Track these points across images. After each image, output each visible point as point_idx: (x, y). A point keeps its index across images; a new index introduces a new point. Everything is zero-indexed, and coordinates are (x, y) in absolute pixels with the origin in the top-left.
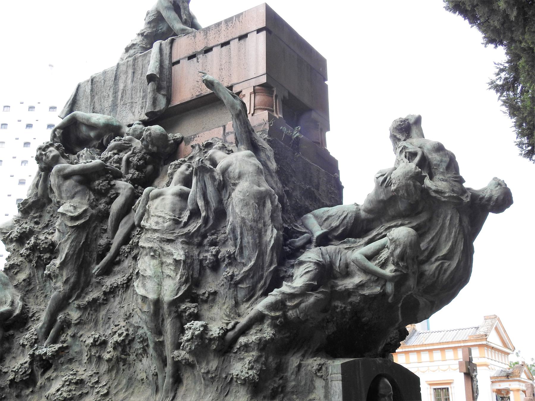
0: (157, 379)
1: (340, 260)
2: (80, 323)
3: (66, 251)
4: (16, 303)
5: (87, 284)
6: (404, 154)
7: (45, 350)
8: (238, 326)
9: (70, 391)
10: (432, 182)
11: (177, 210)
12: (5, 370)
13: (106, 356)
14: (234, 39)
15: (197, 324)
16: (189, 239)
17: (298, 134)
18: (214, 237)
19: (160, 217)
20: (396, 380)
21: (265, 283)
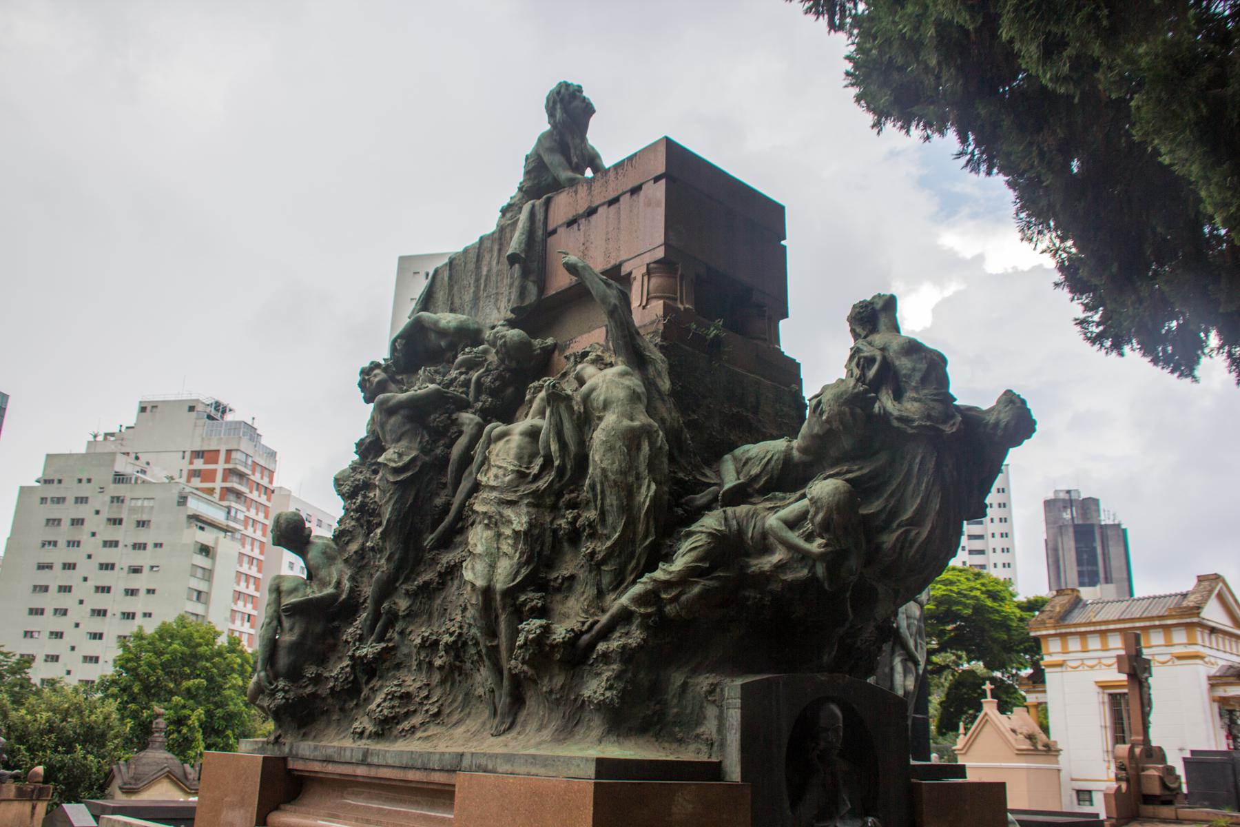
5: (419, 561)
7: (365, 651)
9: (393, 707)
12: (327, 674)
13: (438, 662)
14: (624, 193)
15: (533, 626)
16: (537, 500)
18: (573, 495)
19: (500, 467)
21: (638, 563)
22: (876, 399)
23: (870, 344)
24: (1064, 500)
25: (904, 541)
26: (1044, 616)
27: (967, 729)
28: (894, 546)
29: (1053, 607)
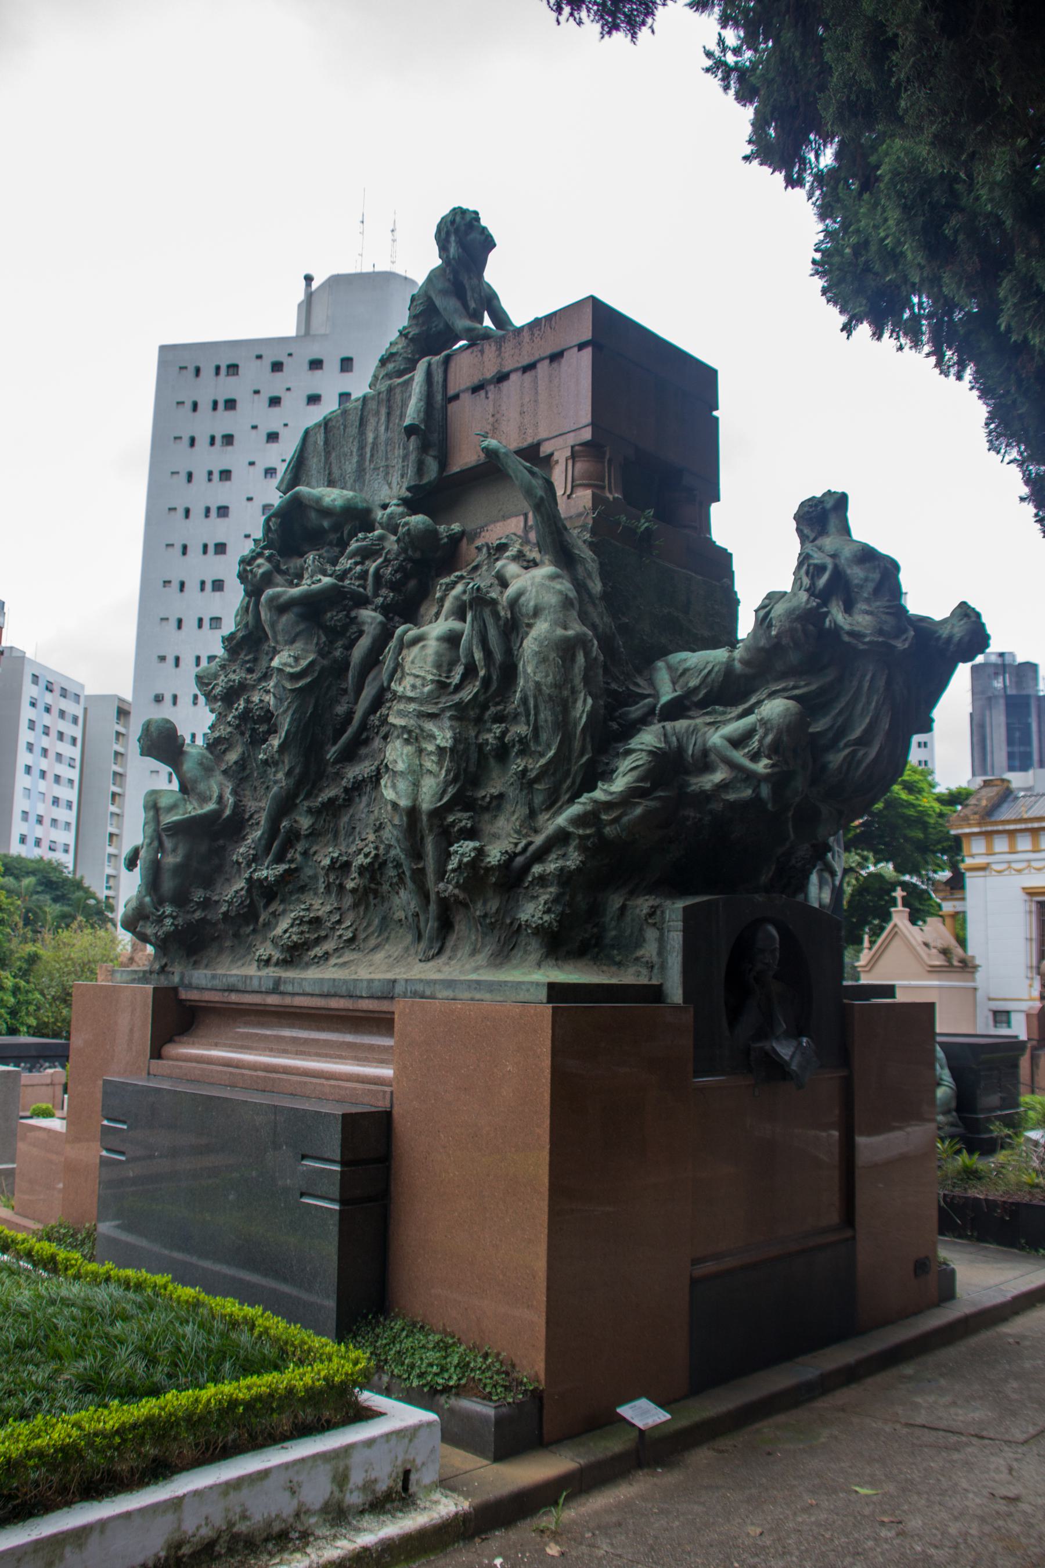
0: (419, 921)
1: (695, 745)
2: (314, 834)
3: (286, 727)
4: (226, 799)
5: (321, 775)
6: (805, 567)
7: (265, 873)
8: (532, 848)
9: (302, 933)
10: (846, 616)
11: (445, 664)
12: (216, 898)
13: (350, 885)
14: (542, 359)
15: (467, 846)
16: (460, 713)
17: (646, 525)
18: (500, 708)
19: (417, 676)
20: (791, 927)
21: (573, 783)
22: (827, 614)
23: (820, 549)
24: (995, 665)
25: (851, 761)
26: (967, 811)
27: (872, 943)
28: (841, 765)
29: (979, 800)
